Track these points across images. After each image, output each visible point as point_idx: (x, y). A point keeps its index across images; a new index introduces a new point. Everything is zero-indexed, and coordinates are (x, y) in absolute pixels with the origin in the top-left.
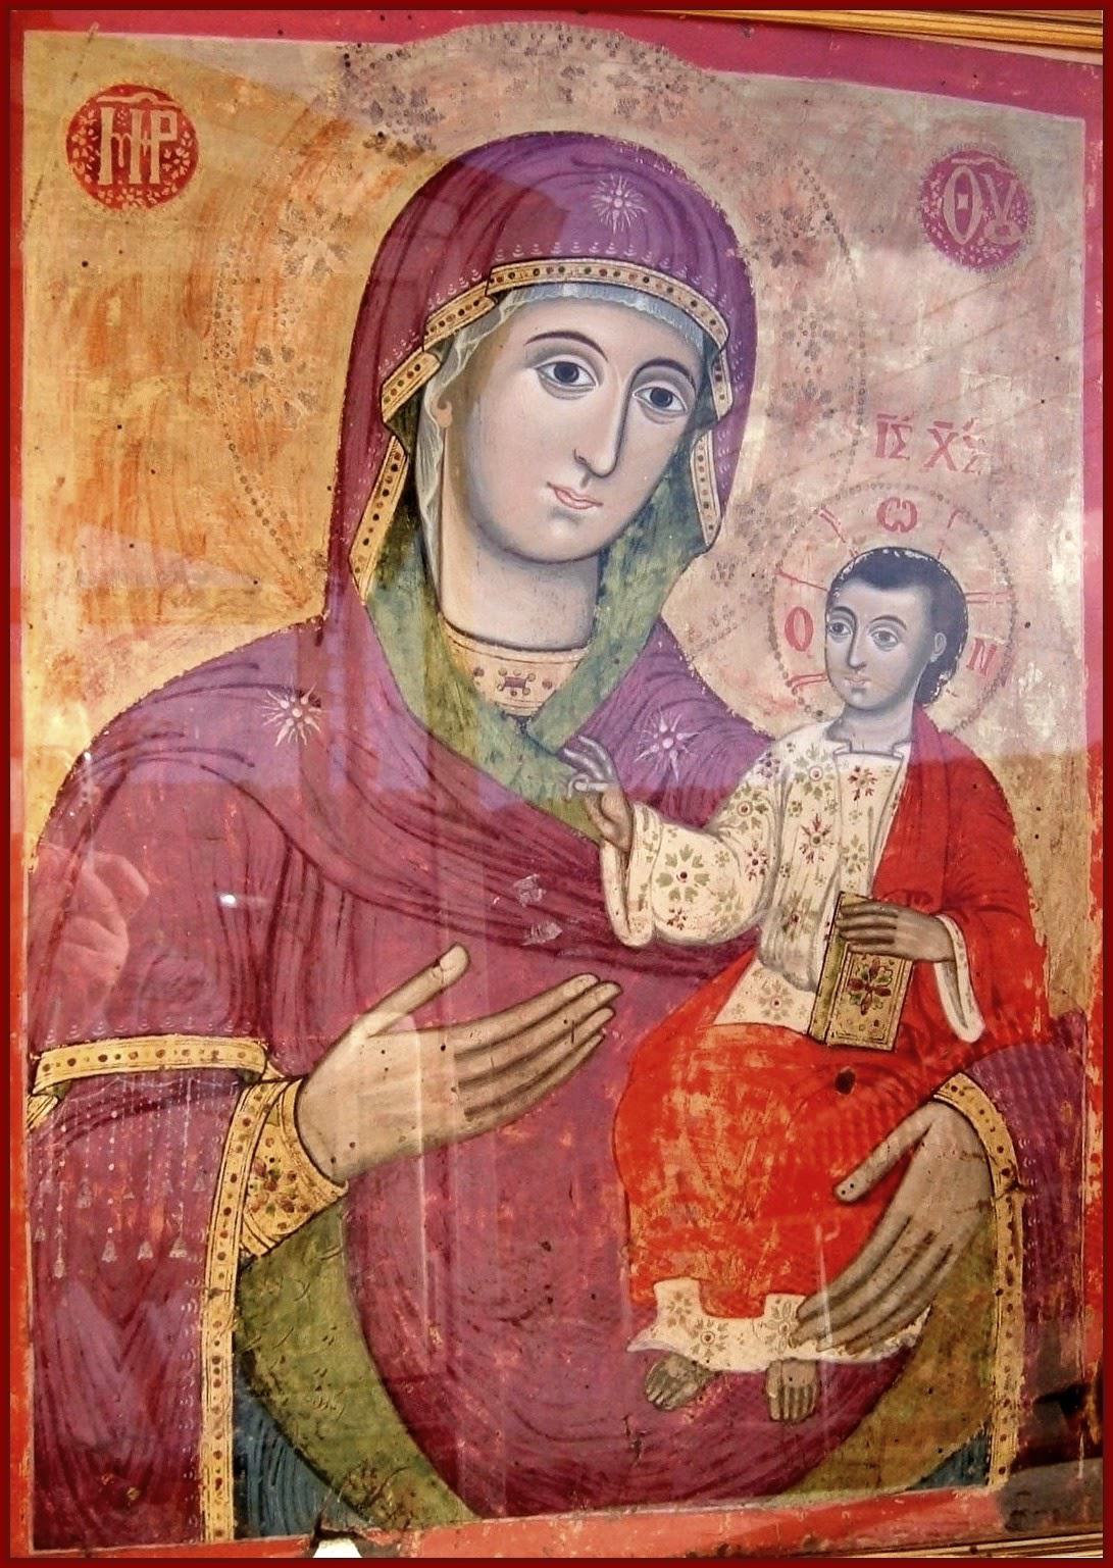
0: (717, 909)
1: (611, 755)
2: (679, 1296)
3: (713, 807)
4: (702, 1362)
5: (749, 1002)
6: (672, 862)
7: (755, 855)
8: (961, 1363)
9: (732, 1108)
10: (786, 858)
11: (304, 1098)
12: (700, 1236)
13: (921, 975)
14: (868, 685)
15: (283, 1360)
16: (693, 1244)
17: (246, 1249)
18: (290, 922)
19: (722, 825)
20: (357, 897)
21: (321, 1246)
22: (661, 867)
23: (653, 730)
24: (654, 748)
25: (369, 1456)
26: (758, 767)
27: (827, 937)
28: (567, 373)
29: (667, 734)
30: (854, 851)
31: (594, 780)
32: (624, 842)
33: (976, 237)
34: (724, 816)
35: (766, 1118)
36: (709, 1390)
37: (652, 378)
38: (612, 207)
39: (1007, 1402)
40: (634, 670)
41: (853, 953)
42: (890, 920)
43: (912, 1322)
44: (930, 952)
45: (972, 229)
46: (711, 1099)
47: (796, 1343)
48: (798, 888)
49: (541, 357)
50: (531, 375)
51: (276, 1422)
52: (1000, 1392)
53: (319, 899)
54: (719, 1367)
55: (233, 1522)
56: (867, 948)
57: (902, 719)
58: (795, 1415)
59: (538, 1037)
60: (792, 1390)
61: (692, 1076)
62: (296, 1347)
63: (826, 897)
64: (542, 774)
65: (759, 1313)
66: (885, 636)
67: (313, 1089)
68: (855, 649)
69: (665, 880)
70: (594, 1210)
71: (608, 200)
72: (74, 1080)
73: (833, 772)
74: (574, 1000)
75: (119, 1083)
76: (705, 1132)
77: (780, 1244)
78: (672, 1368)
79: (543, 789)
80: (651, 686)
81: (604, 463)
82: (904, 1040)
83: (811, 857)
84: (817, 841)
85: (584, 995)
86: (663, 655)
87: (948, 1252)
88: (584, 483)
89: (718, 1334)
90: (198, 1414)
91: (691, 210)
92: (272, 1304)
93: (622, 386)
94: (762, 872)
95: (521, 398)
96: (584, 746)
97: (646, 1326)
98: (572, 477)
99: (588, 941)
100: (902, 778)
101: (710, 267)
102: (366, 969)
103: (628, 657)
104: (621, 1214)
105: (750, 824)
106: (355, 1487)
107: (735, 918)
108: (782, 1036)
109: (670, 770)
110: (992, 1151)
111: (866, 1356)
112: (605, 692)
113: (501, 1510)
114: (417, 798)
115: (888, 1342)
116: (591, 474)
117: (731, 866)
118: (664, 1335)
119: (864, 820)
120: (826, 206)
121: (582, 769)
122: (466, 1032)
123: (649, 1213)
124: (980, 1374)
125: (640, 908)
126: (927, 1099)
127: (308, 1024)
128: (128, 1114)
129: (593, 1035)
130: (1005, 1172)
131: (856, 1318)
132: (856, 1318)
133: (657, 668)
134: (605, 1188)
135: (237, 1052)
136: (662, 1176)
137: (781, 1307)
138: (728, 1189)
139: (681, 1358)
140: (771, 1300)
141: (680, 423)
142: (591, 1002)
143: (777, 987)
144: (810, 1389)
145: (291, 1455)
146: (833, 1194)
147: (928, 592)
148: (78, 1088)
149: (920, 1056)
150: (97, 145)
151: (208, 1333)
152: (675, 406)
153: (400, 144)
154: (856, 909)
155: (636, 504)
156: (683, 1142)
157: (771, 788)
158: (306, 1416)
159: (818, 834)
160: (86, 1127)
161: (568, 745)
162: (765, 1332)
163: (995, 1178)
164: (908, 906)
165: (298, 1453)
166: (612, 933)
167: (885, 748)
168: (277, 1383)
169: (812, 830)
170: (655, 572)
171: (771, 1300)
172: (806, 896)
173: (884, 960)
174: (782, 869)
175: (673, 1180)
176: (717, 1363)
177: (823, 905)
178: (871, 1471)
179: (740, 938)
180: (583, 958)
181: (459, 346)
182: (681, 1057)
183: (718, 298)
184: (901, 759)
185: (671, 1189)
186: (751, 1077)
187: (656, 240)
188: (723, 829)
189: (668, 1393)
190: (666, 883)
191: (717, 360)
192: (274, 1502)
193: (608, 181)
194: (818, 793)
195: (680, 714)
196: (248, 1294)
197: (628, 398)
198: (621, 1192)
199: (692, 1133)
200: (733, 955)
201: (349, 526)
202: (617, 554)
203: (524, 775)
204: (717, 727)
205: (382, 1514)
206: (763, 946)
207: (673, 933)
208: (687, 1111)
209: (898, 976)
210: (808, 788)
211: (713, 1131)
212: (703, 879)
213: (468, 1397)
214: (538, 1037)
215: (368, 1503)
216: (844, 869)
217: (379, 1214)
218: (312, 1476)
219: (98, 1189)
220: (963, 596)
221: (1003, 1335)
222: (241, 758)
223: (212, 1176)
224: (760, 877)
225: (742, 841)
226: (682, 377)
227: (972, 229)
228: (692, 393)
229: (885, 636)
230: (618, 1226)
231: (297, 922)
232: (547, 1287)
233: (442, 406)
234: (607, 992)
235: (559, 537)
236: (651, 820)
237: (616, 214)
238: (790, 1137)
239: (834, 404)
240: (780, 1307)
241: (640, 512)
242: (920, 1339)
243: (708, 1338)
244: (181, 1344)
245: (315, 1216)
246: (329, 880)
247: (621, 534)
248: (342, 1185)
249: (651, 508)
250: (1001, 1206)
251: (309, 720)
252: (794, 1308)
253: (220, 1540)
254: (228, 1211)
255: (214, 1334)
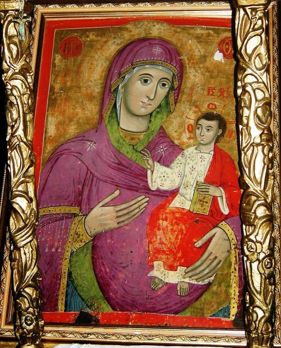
0: (171, 183)
1: (151, 152)
2: (159, 265)
3: (171, 163)
4: (163, 280)
5: (176, 203)
6: (162, 174)
7: (179, 173)
8: (223, 288)
9: (172, 225)
10: (186, 174)
11: (86, 219)
12: (164, 252)
13: (215, 199)
14: (204, 139)
15: (77, 274)
16: (162, 254)
17: (73, 250)
18: (86, 185)
19: (173, 166)
20: (99, 180)
21: (87, 250)
22: (159, 174)
23: (159, 148)
24: (159, 151)
25: (92, 295)
26: (180, 155)
27: (194, 190)
28: (146, 81)
29: (162, 148)
30: (201, 173)
31: (147, 157)
32: (152, 169)
33: (229, 53)
34: (173, 165)
35: (179, 227)
36: (164, 287)
37: (162, 81)
38: (156, 51)
39: (234, 299)
40: (156, 136)
41: (200, 194)
42: (208, 187)
43: (212, 277)
44: (217, 195)
45: (229, 52)
46: (168, 223)
47: (184, 278)
48: (188, 180)
49: (141, 78)
50: (139, 81)
51: (75, 287)
52: (233, 296)
53: (92, 180)
54: (167, 282)
55: (64, 308)
56: (203, 193)
57: (212, 146)
58: (184, 295)
59: (133, 208)
60: (183, 289)
61: (164, 218)
62: (80, 271)
63: (194, 182)
64: (137, 156)
65: (176, 270)
66: (208, 130)
67: (88, 218)
68: (202, 133)
69: (160, 177)
70: (142, 245)
71: (155, 50)
72: (44, 215)
73: (196, 156)
74: (140, 201)
75: (52, 216)
76: (166, 230)
77: (181, 255)
78: (157, 281)
79: (137, 159)
80: (159, 139)
81: (152, 97)
82: (211, 213)
83: (191, 174)
84: (193, 170)
85: (142, 200)
86: (163, 134)
87: (220, 261)
88: (148, 101)
89: (167, 274)
90: (60, 284)
91: (171, 50)
92: (76, 262)
93: (156, 83)
94: (181, 176)
95: (138, 86)
96: (145, 150)
97: (152, 271)
98: (146, 100)
99: (144, 189)
100: (211, 158)
101: (175, 60)
102: (100, 194)
103: (155, 133)
104: (147, 246)
105: (178, 166)
106: (89, 302)
107: (175, 185)
108: (183, 210)
109: (162, 155)
110: (231, 239)
111: (201, 283)
112: (150, 140)
113: (118, 310)
114: (112, 160)
115: (206, 280)
116: (150, 99)
117: (174, 175)
118: (154, 273)
119: (203, 166)
120: (198, 49)
121: (145, 155)
122: (119, 206)
123: (153, 246)
124: (228, 291)
125: (155, 183)
126: (216, 226)
127: (88, 204)
128: (53, 222)
129: (144, 208)
130: (234, 244)
131: (198, 274)
132: (198, 274)
133: (160, 136)
134: (144, 240)
135: (75, 210)
136: (156, 238)
137: (181, 269)
138: (170, 242)
139: (159, 278)
140: (179, 267)
141: (168, 89)
142: (144, 201)
143: (183, 200)
144: (187, 288)
145: (77, 295)
146: (194, 245)
147: (218, 121)
148: (45, 217)
149: (215, 218)
150: (65, 47)
151: (64, 267)
152: (167, 86)
153: (118, 43)
154: (201, 185)
155: (158, 104)
156: (161, 231)
157: (183, 159)
158: (81, 286)
159: (193, 169)
160: (45, 224)
161: (142, 150)
162: (178, 275)
163: (232, 246)
164: (212, 185)
165: (78, 294)
166: (149, 187)
167: (208, 152)
168: (76, 278)
169: (192, 168)
170: (161, 117)
171: (179, 267)
172: (190, 181)
173: (207, 196)
174: (185, 176)
175: (159, 239)
176: (166, 281)
177: (193, 184)
178: (201, 311)
179: (175, 189)
180: (142, 192)
181: (126, 77)
182: (162, 213)
183: (176, 66)
184: (211, 154)
185: (158, 241)
186: (176, 218)
187: (164, 56)
188: (173, 167)
189: (155, 286)
190: (160, 177)
191: (175, 77)
192: (72, 305)
193: (156, 46)
194: (193, 161)
195: (164, 145)
196: (72, 259)
197: (157, 85)
198: (148, 241)
199: (163, 229)
200: (174, 193)
201: (104, 111)
202: (154, 114)
203: (133, 156)
204: (172, 147)
205: (94, 308)
206: (180, 191)
207: (162, 188)
208: (162, 225)
209: (209, 200)
210: (191, 159)
211: (168, 229)
212: (168, 177)
213: (113, 284)
214: (133, 208)
215: (91, 306)
216: (198, 176)
217: (99, 244)
218: (81, 299)
219: (46, 237)
220: (226, 122)
221: (234, 282)
222: (80, 153)
223: (67, 235)
224: (180, 177)
225: (176, 170)
226: (169, 82)
227: (229, 52)
228: (170, 84)
229: (208, 130)
230: (147, 249)
231: (88, 185)
232: (131, 261)
233: (122, 88)
234: (147, 199)
235: (143, 111)
236: (158, 165)
237: (157, 52)
238: (184, 232)
239: (199, 86)
240: (181, 269)
241: (159, 106)
242: (213, 281)
243: (165, 275)
244: (58, 269)
245: (87, 243)
246: (95, 177)
247: (155, 110)
248: (92, 237)
249: (161, 105)
250: (233, 252)
251: (93, 146)
252: (184, 271)
253: (62, 312)
254: (70, 242)
255: (65, 267)
